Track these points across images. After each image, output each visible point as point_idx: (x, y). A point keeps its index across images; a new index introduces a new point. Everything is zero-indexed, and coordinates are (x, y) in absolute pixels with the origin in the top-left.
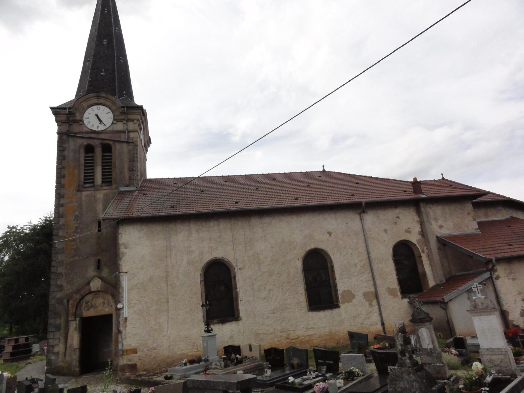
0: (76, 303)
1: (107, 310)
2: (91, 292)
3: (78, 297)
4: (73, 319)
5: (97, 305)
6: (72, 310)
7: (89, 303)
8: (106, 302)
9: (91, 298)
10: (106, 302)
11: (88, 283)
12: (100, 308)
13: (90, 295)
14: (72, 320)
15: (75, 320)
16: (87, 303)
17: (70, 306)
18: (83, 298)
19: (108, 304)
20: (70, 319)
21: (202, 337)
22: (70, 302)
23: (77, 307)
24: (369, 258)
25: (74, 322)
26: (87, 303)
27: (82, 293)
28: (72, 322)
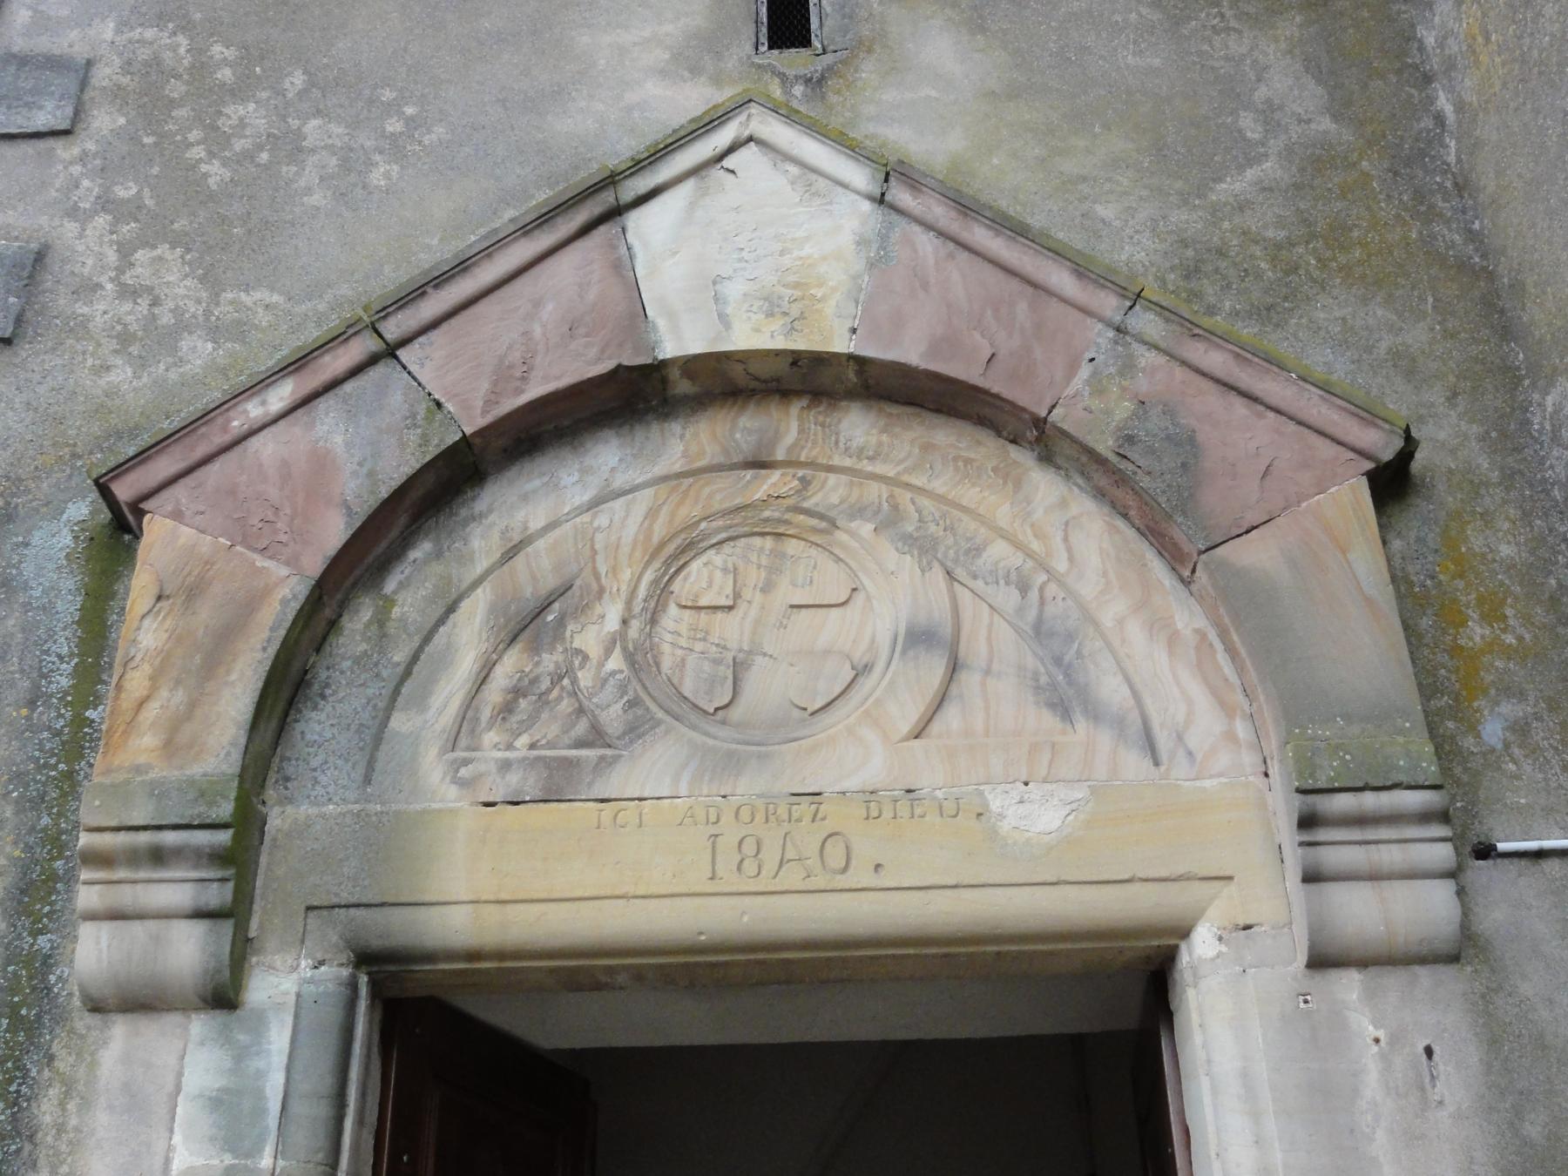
0: (285, 588)
1: (1036, 816)
2: (635, 394)
3: (361, 449)
4: (187, 950)
5: (770, 687)
6: (175, 724)
7: (589, 638)
8: (993, 636)
9: (626, 523)
10: (993, 636)
11: (600, 203)
12: (856, 757)
13: (607, 458)
14: (138, 1001)
15: (222, 997)
16: (529, 623)
17: (145, 633)
18: (453, 478)
19: (1065, 695)
20: (93, 952)
21: (89, 63)
22: (162, 538)
23: (287, 690)
24: (1217, 381)
25: (193, 1056)
26: (529, 623)
27: (467, 376)
28: (118, 1047)
